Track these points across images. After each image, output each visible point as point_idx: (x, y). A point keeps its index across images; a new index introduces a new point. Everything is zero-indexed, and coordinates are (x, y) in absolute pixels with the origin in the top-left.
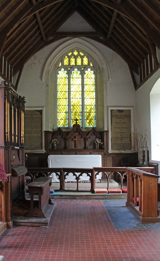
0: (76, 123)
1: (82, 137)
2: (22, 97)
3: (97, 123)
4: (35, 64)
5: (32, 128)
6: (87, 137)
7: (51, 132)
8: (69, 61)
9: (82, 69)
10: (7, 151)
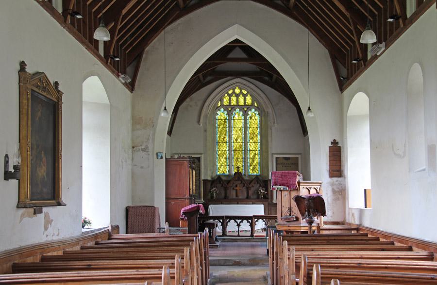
0: (238, 171)
1: (244, 186)
3: (262, 170)
4: (191, 106)
6: (251, 186)
7: (210, 181)
8: (230, 100)
9: (245, 109)
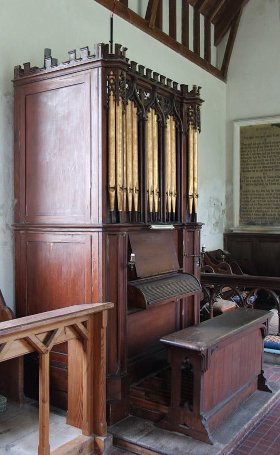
2: (190, 89)
5: (265, 171)
10: (113, 237)
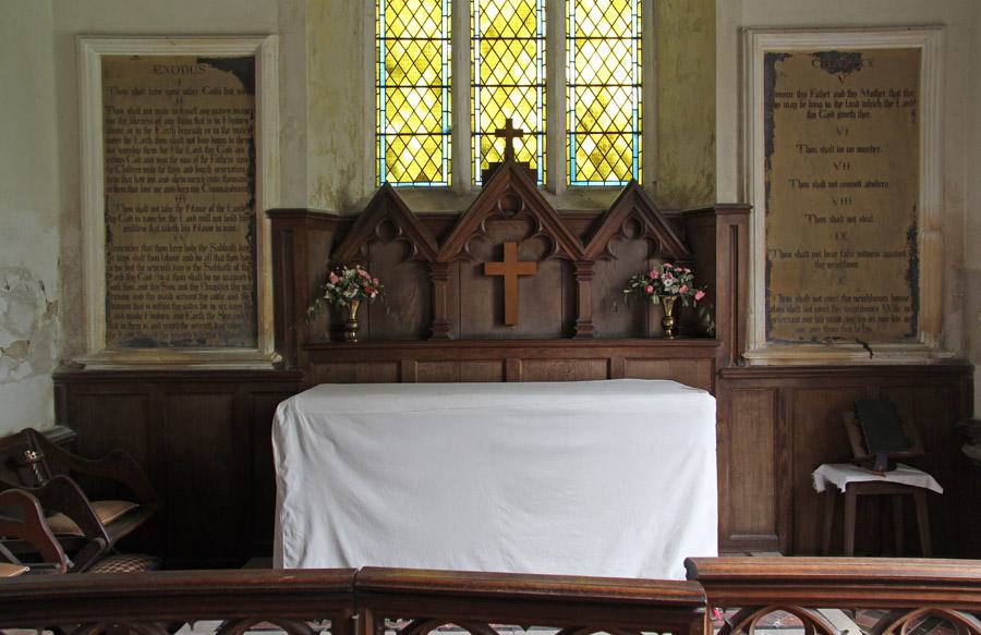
1: (529, 234)
6: (589, 252)
7: (321, 219)
